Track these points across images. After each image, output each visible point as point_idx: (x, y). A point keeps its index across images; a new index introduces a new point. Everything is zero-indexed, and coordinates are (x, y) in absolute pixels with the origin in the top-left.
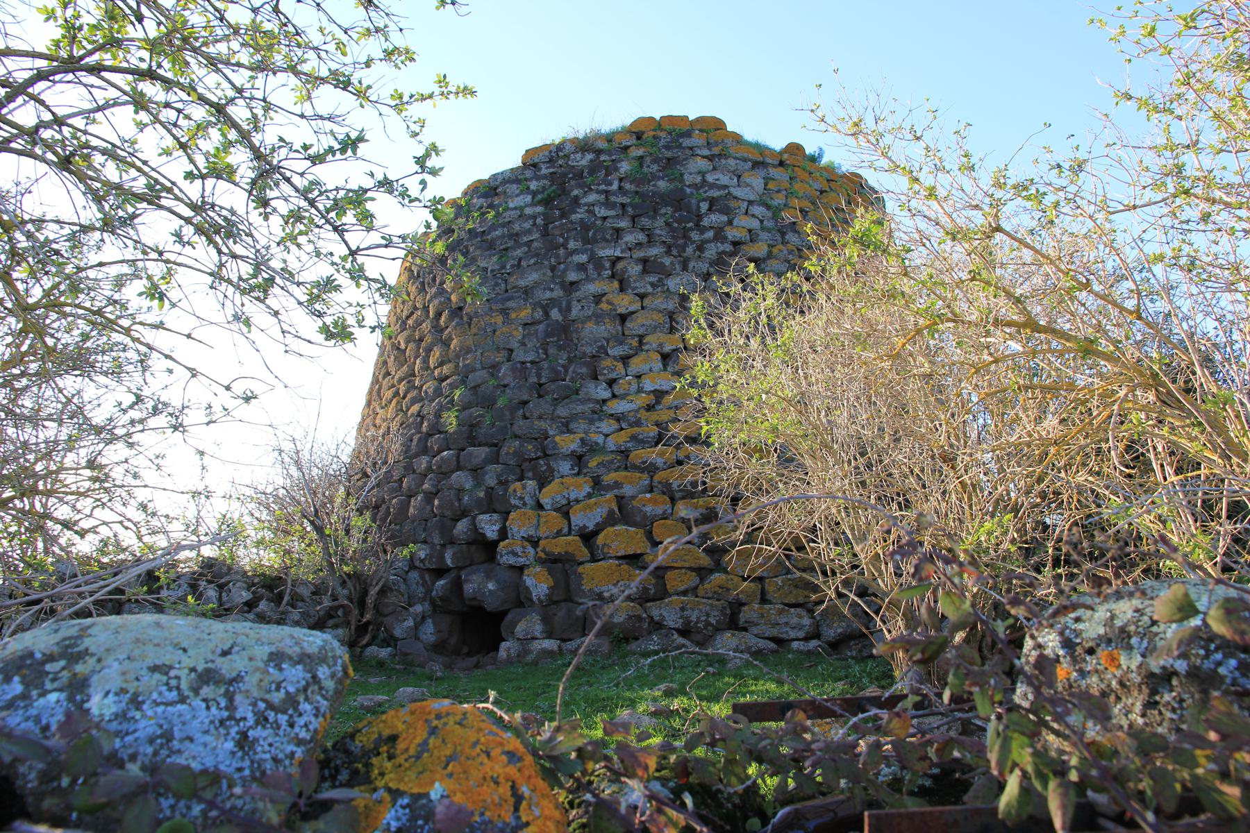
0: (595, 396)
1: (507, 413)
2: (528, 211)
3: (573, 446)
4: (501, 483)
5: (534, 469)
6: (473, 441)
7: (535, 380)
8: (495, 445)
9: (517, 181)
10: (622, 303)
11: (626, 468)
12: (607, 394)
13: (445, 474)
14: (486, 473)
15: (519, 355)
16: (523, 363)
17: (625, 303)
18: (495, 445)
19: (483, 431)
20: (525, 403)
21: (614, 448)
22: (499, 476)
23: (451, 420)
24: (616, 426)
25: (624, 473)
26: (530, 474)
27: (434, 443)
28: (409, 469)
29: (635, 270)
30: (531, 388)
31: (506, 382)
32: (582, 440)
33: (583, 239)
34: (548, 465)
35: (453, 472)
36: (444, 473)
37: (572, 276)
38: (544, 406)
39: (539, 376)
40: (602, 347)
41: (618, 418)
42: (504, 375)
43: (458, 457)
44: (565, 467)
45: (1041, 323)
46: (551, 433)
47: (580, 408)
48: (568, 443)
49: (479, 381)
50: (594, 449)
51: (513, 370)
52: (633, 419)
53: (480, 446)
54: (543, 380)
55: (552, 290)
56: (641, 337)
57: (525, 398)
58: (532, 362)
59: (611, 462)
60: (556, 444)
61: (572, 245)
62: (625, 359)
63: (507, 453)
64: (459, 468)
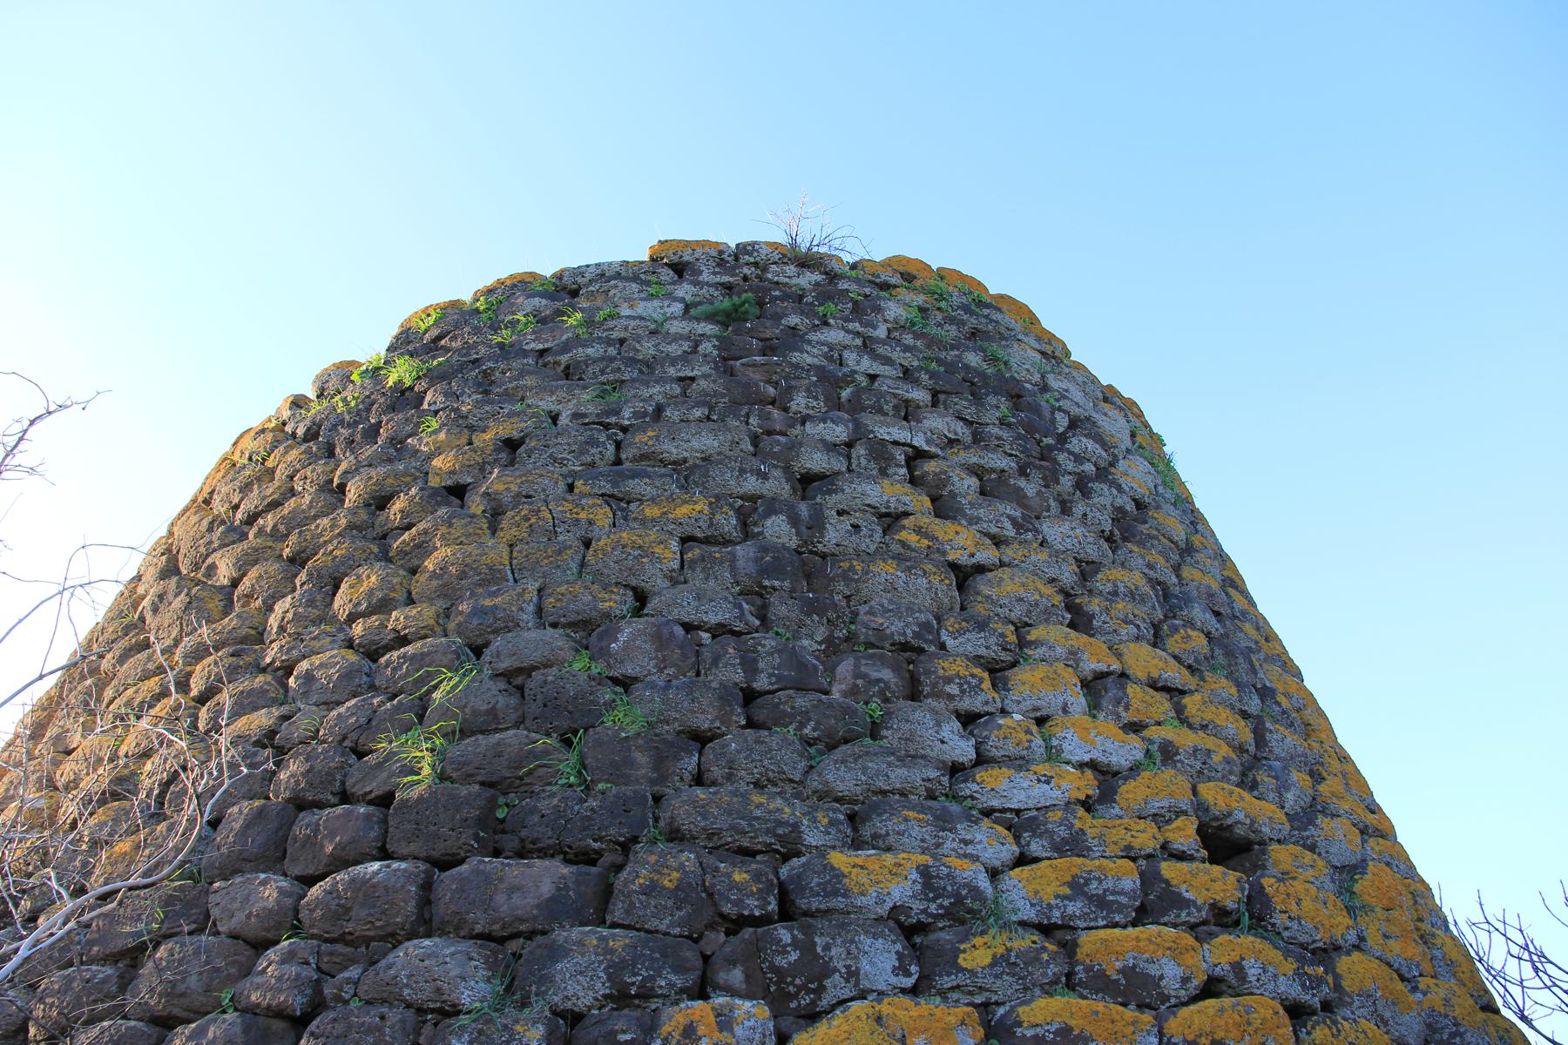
0: (936, 750)
1: (642, 758)
2: (676, 327)
3: (901, 891)
4: (621, 998)
5: (752, 957)
6: (500, 837)
7: (739, 676)
8: (587, 858)
9: (635, 278)
10: (960, 540)
11: (1071, 986)
12: (964, 750)
13: (357, 940)
14: (557, 952)
15: (677, 604)
16: (689, 627)
17: (962, 542)
18: (587, 858)
19: (544, 805)
20: (701, 739)
21: (1029, 914)
22: (615, 971)
23: (416, 762)
24: (1009, 850)
25: (1073, 1000)
26: (736, 976)
27: (331, 826)
28: (189, 910)
29: (966, 485)
30: (724, 695)
31: (630, 670)
32: (924, 872)
33: (827, 400)
34: (807, 948)
35: (393, 939)
36: (357, 940)
37: (816, 461)
38: (780, 749)
39: (750, 666)
40: (925, 626)
41: (1017, 822)
42: (627, 647)
43: (427, 886)
44: (880, 960)
45: (326, 991)
46: (812, 838)
47: (898, 776)
48: (883, 878)
49: (536, 657)
50: (965, 912)
51: (660, 639)
52: (1063, 832)
53: (521, 854)
54: (761, 683)
55: (764, 476)
56: (1021, 627)
57: (704, 722)
58: (719, 631)
59: (1032, 958)
60: (839, 876)
61: (799, 402)
62: (997, 671)
63: (650, 890)
64: (425, 924)
